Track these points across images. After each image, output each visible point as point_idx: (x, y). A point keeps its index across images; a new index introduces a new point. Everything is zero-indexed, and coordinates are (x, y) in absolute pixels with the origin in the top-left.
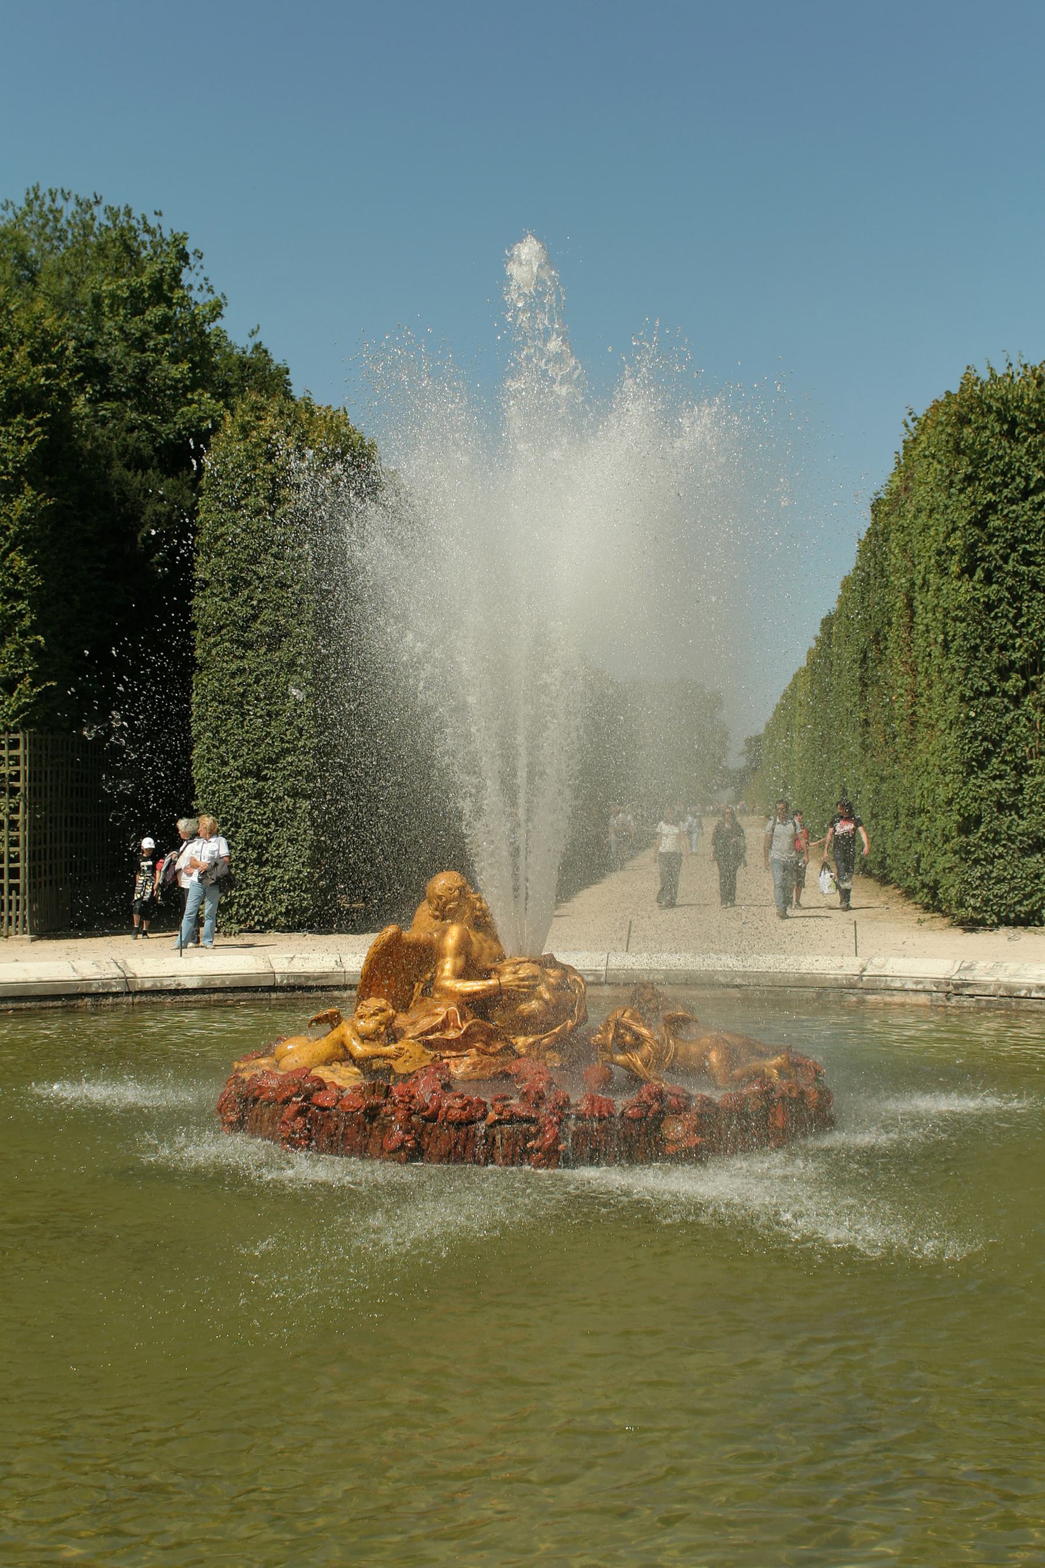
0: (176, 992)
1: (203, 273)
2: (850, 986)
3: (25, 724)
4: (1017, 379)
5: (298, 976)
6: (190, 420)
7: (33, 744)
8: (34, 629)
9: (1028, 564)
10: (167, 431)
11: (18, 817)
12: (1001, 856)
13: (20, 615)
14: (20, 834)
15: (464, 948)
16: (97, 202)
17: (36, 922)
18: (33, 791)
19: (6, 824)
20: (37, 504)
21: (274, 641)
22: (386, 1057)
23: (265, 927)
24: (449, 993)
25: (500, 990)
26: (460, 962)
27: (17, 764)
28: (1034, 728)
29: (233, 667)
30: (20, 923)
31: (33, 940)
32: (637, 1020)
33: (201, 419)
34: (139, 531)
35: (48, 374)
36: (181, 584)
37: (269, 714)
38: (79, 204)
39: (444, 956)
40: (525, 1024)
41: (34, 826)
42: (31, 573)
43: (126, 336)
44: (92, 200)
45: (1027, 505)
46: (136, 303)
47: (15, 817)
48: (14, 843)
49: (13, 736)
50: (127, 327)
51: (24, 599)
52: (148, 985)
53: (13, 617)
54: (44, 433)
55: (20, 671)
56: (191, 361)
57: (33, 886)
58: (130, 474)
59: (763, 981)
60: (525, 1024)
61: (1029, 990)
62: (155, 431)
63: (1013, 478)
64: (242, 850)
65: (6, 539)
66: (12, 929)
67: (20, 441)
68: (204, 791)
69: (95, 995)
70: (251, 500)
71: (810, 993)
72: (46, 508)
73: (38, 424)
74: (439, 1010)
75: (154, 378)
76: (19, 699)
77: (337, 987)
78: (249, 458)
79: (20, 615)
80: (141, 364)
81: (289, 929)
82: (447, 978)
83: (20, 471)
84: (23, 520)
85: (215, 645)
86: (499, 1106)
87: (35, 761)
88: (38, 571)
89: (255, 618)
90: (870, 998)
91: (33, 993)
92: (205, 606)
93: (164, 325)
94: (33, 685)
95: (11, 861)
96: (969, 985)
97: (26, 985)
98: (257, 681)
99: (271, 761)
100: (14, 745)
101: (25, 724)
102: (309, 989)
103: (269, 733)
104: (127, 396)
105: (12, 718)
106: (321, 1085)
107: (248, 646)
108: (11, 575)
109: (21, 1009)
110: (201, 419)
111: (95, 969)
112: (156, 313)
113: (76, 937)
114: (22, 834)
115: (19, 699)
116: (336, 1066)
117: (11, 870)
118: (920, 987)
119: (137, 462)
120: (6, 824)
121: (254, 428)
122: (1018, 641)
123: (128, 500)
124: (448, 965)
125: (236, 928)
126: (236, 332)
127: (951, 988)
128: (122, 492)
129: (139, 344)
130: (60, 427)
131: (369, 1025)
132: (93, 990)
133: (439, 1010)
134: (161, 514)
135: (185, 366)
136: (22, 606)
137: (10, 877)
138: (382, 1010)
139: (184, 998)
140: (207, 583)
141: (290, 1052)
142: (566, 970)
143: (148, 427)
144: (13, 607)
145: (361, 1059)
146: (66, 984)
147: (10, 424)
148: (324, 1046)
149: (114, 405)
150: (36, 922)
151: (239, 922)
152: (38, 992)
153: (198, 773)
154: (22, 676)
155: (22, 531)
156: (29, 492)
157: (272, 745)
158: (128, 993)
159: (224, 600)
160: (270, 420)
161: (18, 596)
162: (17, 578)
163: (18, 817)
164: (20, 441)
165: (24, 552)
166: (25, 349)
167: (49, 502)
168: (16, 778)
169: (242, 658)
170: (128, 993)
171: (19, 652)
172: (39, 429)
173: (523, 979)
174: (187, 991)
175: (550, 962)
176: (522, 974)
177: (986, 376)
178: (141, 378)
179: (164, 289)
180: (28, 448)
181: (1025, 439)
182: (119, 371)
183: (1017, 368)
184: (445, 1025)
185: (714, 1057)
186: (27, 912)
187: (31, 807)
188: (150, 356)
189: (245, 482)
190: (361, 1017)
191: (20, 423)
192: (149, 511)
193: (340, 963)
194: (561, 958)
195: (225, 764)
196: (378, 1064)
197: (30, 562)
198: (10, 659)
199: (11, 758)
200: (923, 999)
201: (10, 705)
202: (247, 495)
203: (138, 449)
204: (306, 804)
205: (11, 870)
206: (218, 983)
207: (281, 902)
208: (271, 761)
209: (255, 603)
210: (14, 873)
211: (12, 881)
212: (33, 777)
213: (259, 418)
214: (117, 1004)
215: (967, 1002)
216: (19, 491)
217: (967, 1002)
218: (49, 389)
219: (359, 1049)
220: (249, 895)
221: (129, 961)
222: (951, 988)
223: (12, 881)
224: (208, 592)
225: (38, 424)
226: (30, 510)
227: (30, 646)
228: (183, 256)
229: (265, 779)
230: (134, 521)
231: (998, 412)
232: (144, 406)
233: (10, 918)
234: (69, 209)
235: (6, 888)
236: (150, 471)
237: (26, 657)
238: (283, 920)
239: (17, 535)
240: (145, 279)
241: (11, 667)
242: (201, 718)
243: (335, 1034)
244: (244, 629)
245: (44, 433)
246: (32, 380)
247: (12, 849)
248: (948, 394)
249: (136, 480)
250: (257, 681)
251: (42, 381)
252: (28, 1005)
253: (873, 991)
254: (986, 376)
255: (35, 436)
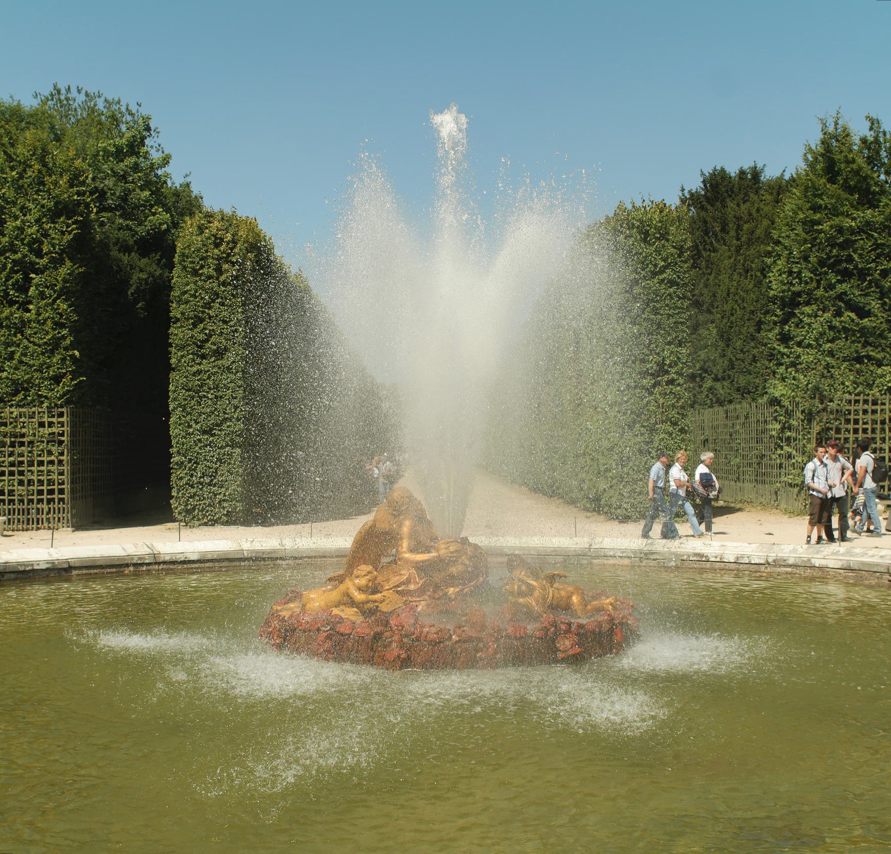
0: (184, 562)
1: (159, 141)
2: (581, 555)
3: (68, 402)
4: (648, 209)
5: (257, 552)
6: (154, 224)
7: (73, 414)
8: (72, 346)
9: (657, 314)
10: (141, 231)
11: (64, 458)
12: (641, 480)
13: (64, 338)
14: (65, 468)
15: (413, 535)
16: (99, 97)
17: (74, 520)
18: (73, 442)
19: (56, 462)
20: (73, 271)
21: (219, 353)
22: (375, 601)
23: (214, 522)
24: (407, 561)
25: (440, 560)
26: (413, 543)
27: (63, 426)
28: (659, 407)
29: (195, 369)
30: (65, 521)
31: (73, 531)
32: (528, 577)
33: (161, 224)
34: (128, 289)
35: (79, 193)
36: (162, 320)
37: (216, 397)
38: (87, 95)
39: (401, 539)
40: (452, 580)
41: (73, 463)
42: (71, 312)
43: (115, 174)
44: (97, 93)
45: (656, 281)
46: (119, 154)
47: (62, 458)
48: (61, 474)
49: (60, 410)
50: (116, 168)
51: (66, 328)
52: (167, 558)
53: (59, 339)
54: (77, 228)
55: (64, 371)
56: (150, 190)
57: (73, 499)
58: (121, 254)
59: (532, 552)
60: (452, 580)
61: (689, 556)
62: (133, 230)
63: (647, 265)
64: (200, 477)
65: (55, 291)
66: (60, 524)
67: (63, 233)
68: (177, 443)
69: (135, 565)
70: (205, 271)
71: (560, 559)
72: (79, 273)
73: (73, 223)
74: (403, 572)
75: (133, 198)
76: (63, 388)
77: (281, 558)
78: (204, 245)
79: (64, 338)
80: (125, 190)
81: (227, 523)
82: (405, 552)
83: (63, 251)
84: (65, 281)
85: (182, 356)
86: (459, 631)
87: (73, 425)
88: (75, 311)
89: (207, 341)
90: (596, 561)
91: (98, 564)
92: (178, 333)
93: (136, 168)
94: (72, 380)
95: (59, 484)
96: (653, 553)
97: (94, 559)
98: (209, 378)
99: (217, 425)
100: (61, 415)
101: (68, 402)
102: (264, 559)
103: (216, 409)
104: (116, 209)
105: (59, 399)
106: (341, 620)
107: (203, 357)
108: (58, 313)
109: (91, 574)
110: (161, 224)
111: (134, 549)
112: (130, 161)
113: (87, 530)
114: (66, 468)
115: (63, 388)
116: (342, 607)
117: (59, 490)
118: (624, 554)
119: (126, 249)
120: (56, 462)
121: (207, 228)
122: (651, 357)
123: (121, 270)
124: (405, 544)
125: (197, 523)
126: (175, 176)
127: (643, 555)
128: (118, 266)
129: (124, 178)
130: (85, 225)
131: (363, 582)
132: (135, 561)
133: (403, 572)
134: (142, 279)
135: (148, 193)
136: (65, 332)
137: (38, 495)
138: (369, 572)
139: (189, 566)
140: (178, 320)
141: (313, 599)
142: (476, 546)
143: (130, 229)
144: (59, 333)
145: (359, 603)
146: (119, 558)
147: (56, 223)
148: (335, 595)
149: (109, 214)
150: (74, 520)
151: (199, 520)
152: (89, 564)
153: (173, 432)
154: (65, 374)
155: (64, 287)
156: (68, 263)
157: (218, 416)
158: (156, 563)
159: (189, 329)
160: (216, 223)
161: (62, 326)
162: (61, 315)
163: (64, 458)
164: (63, 233)
165: (66, 300)
166: (66, 178)
167: (81, 270)
168: (62, 435)
169: (200, 364)
170: (156, 563)
171: (63, 360)
172: (74, 226)
173: (452, 553)
174: (193, 562)
175: (465, 541)
176: (452, 549)
177: (630, 207)
178: (124, 199)
179: (135, 146)
180: (68, 237)
181: (654, 243)
182: (112, 194)
183: (647, 203)
184: (408, 582)
185: (575, 599)
186: (69, 515)
187: (72, 452)
188: (130, 186)
189: (201, 260)
190: (357, 577)
191: (63, 222)
192: (135, 277)
193: (281, 544)
194: (472, 540)
195: (190, 426)
196: (370, 605)
197: (70, 306)
198: (58, 364)
199: (59, 423)
200: (626, 562)
201: (58, 391)
202: (202, 267)
203: (125, 241)
204: (238, 451)
205: (59, 490)
206: (209, 557)
207: (224, 508)
208: (217, 425)
209: (207, 331)
210: (61, 491)
211: (60, 496)
212: (73, 434)
213: (210, 222)
214: (149, 570)
215: (652, 563)
216: (61, 262)
217: (652, 563)
218: (79, 203)
219: (359, 597)
220: (205, 504)
221: (155, 544)
222: (643, 555)
223: (60, 496)
224: (179, 324)
225: (73, 223)
226: (69, 274)
227: (70, 356)
228: (148, 129)
229: (214, 435)
230: (125, 283)
231: (638, 227)
232: (124, 216)
233: (59, 518)
234: (81, 98)
235: (56, 500)
236: (133, 254)
237: (68, 362)
238: (225, 519)
239: (61, 289)
240: (124, 141)
241: (58, 368)
242: (175, 399)
243: (342, 587)
244: (201, 347)
245: (77, 228)
246: (69, 197)
247: (60, 477)
248: (607, 218)
249: (125, 258)
250: (209, 378)
251: (75, 197)
252: (95, 571)
253: (597, 557)
254: (630, 207)
255: (72, 230)
